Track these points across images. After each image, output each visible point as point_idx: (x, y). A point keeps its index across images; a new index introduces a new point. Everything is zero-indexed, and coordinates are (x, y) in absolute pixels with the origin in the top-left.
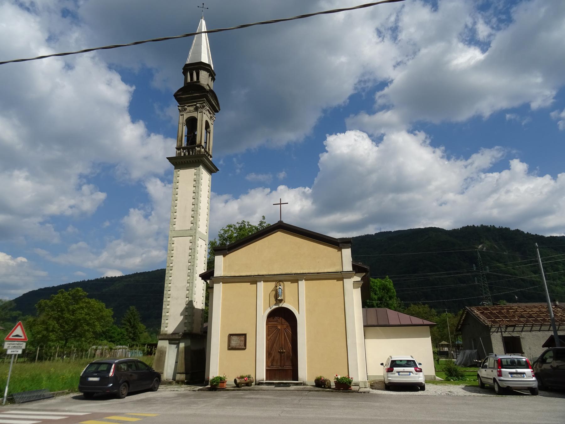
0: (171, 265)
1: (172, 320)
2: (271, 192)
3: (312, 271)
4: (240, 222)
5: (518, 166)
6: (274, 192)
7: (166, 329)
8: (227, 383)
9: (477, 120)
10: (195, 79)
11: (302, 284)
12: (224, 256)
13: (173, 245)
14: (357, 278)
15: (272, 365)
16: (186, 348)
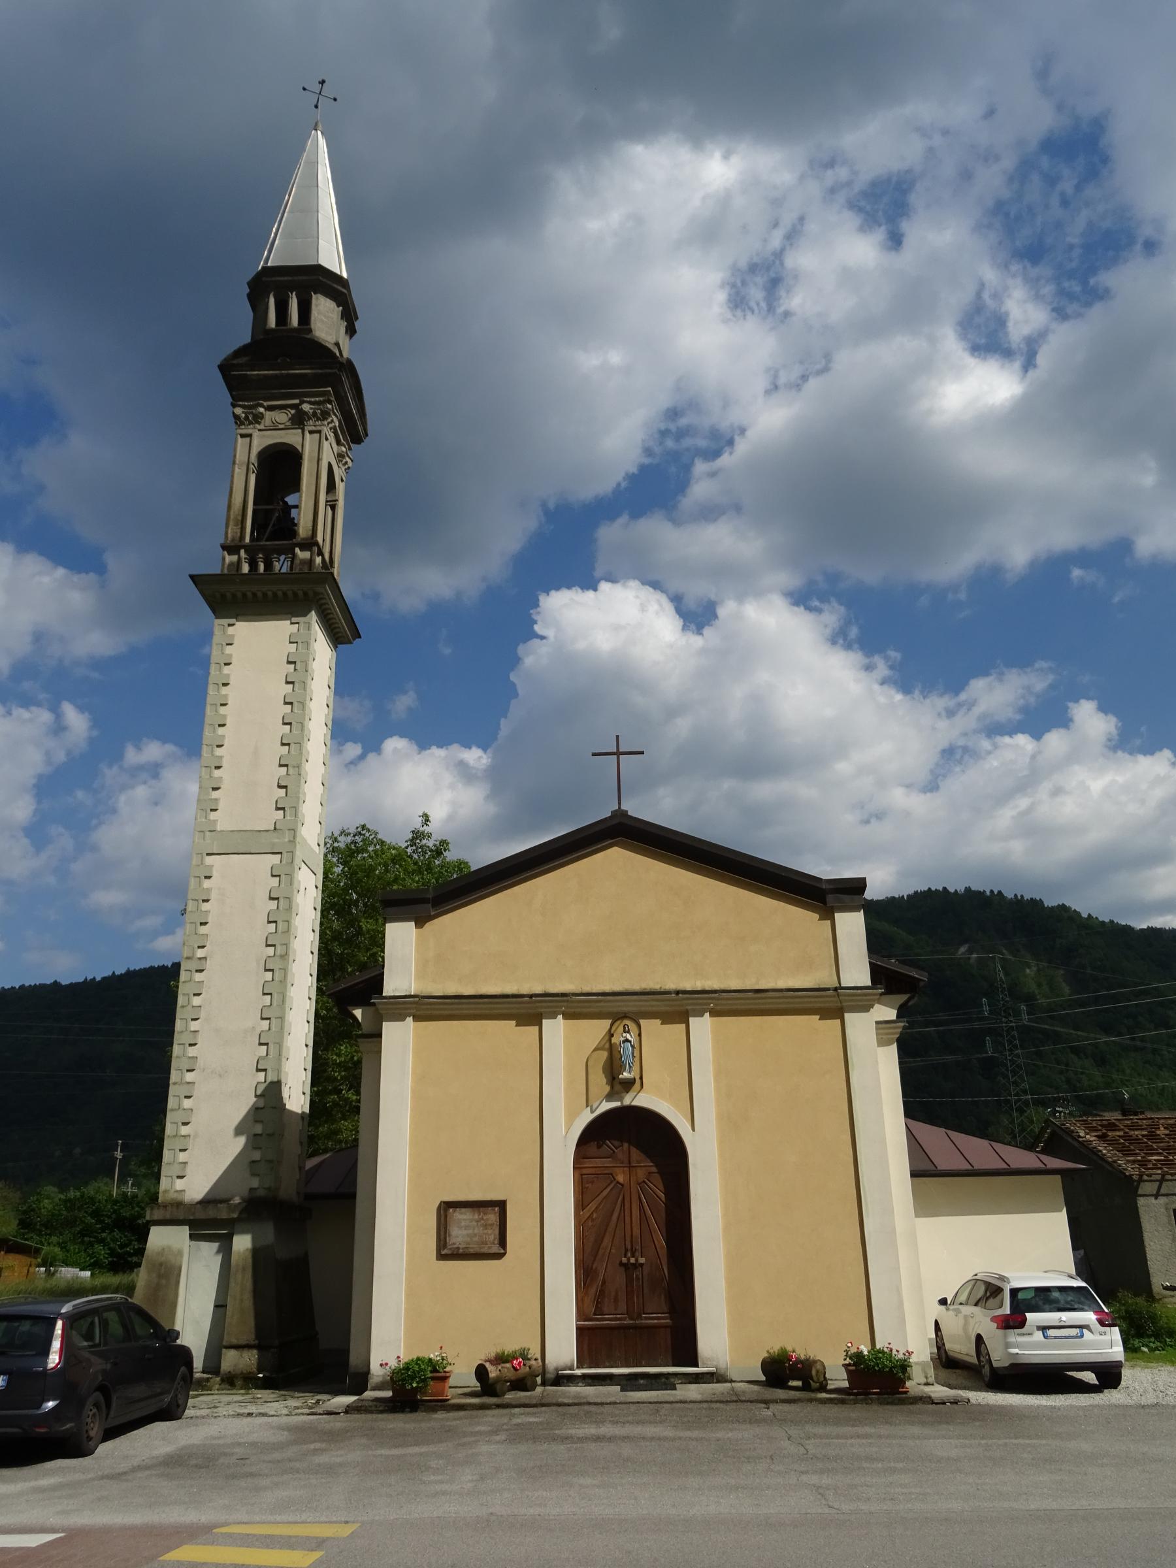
0: (200, 953)
1: (203, 1148)
2: (362, 757)
3: (734, 984)
4: (352, 830)
5: (1091, 721)
6: (371, 757)
7: (179, 1184)
8: (452, 1381)
9: (988, 578)
10: (294, 320)
11: (702, 1027)
12: (420, 923)
13: (207, 884)
14: (886, 1012)
15: (599, 1311)
16: (257, 1252)
